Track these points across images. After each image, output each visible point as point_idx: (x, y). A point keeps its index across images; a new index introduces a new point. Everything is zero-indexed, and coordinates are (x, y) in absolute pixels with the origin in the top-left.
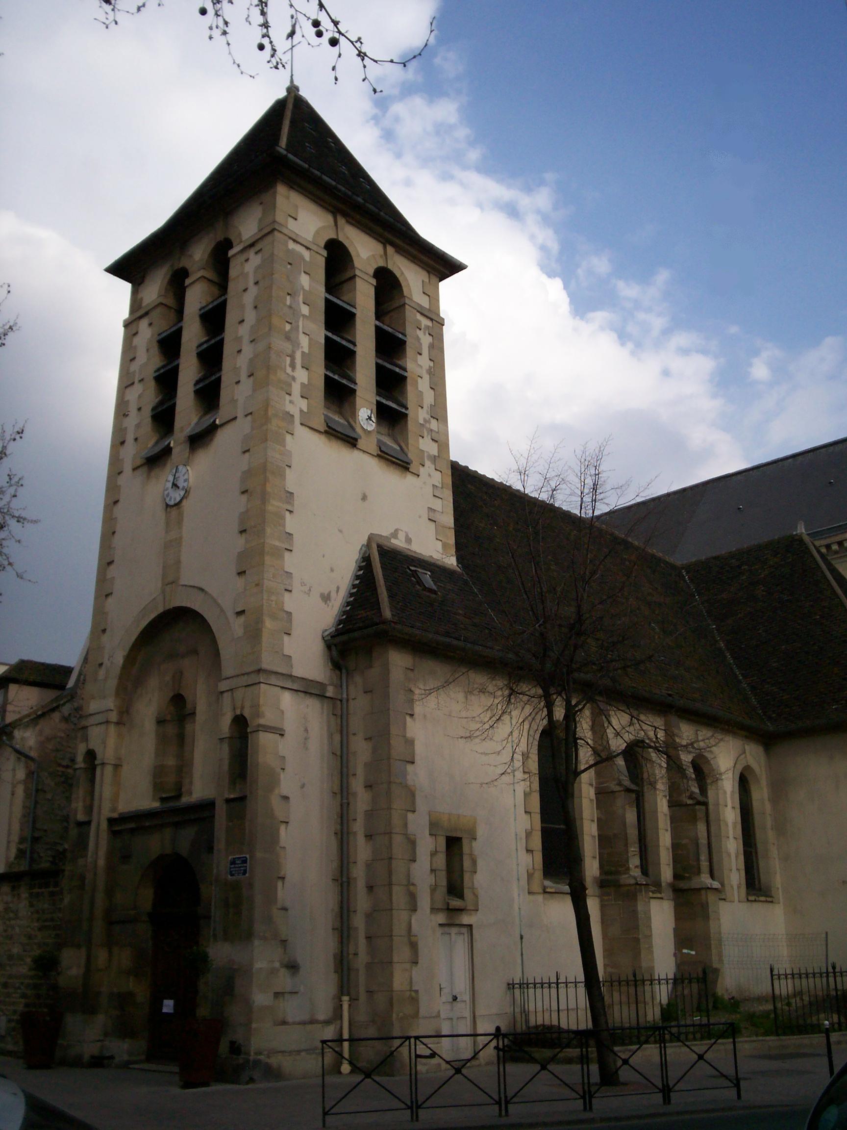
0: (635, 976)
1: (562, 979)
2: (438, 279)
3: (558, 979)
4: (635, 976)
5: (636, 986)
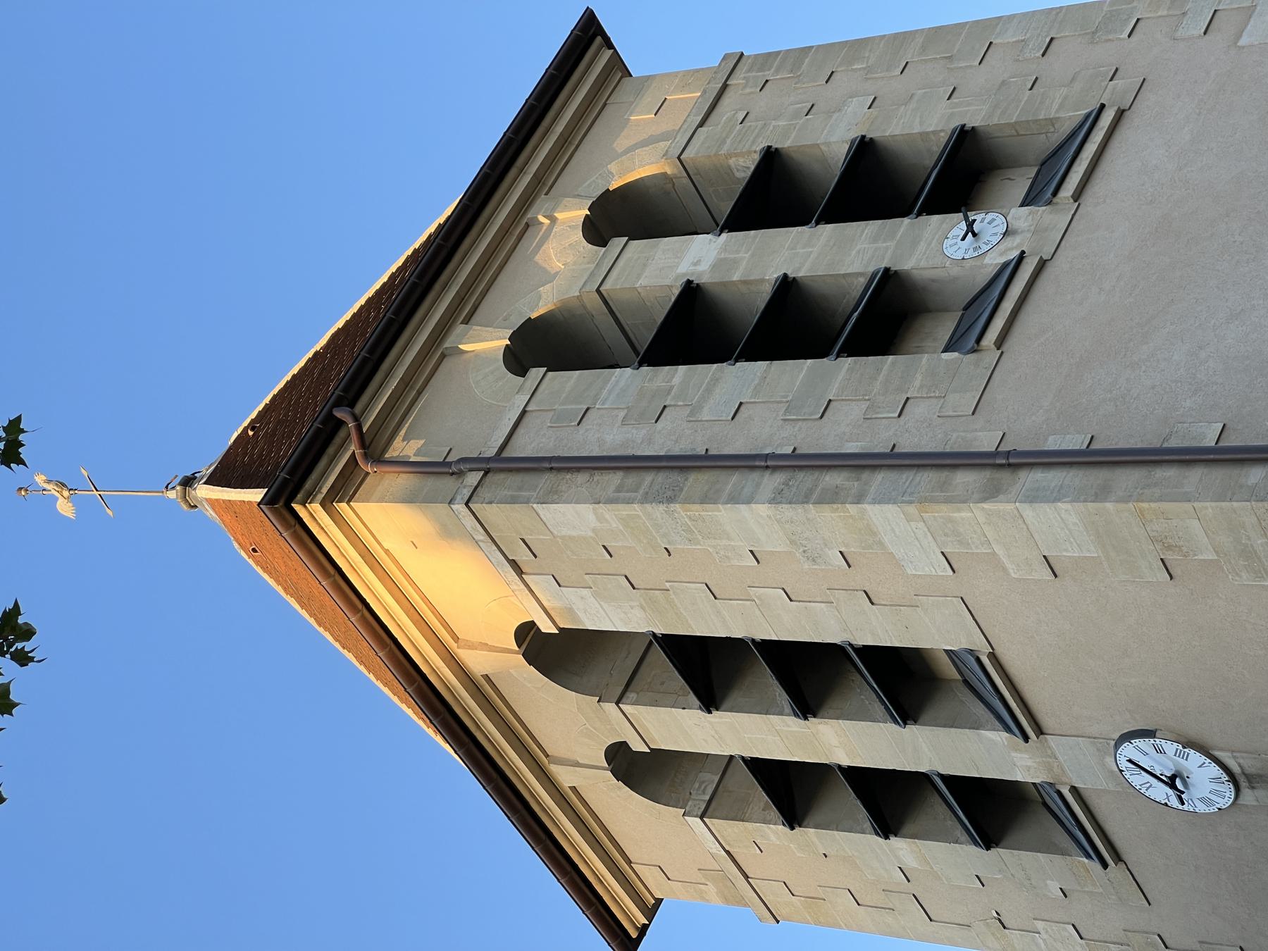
2: (626, 80)
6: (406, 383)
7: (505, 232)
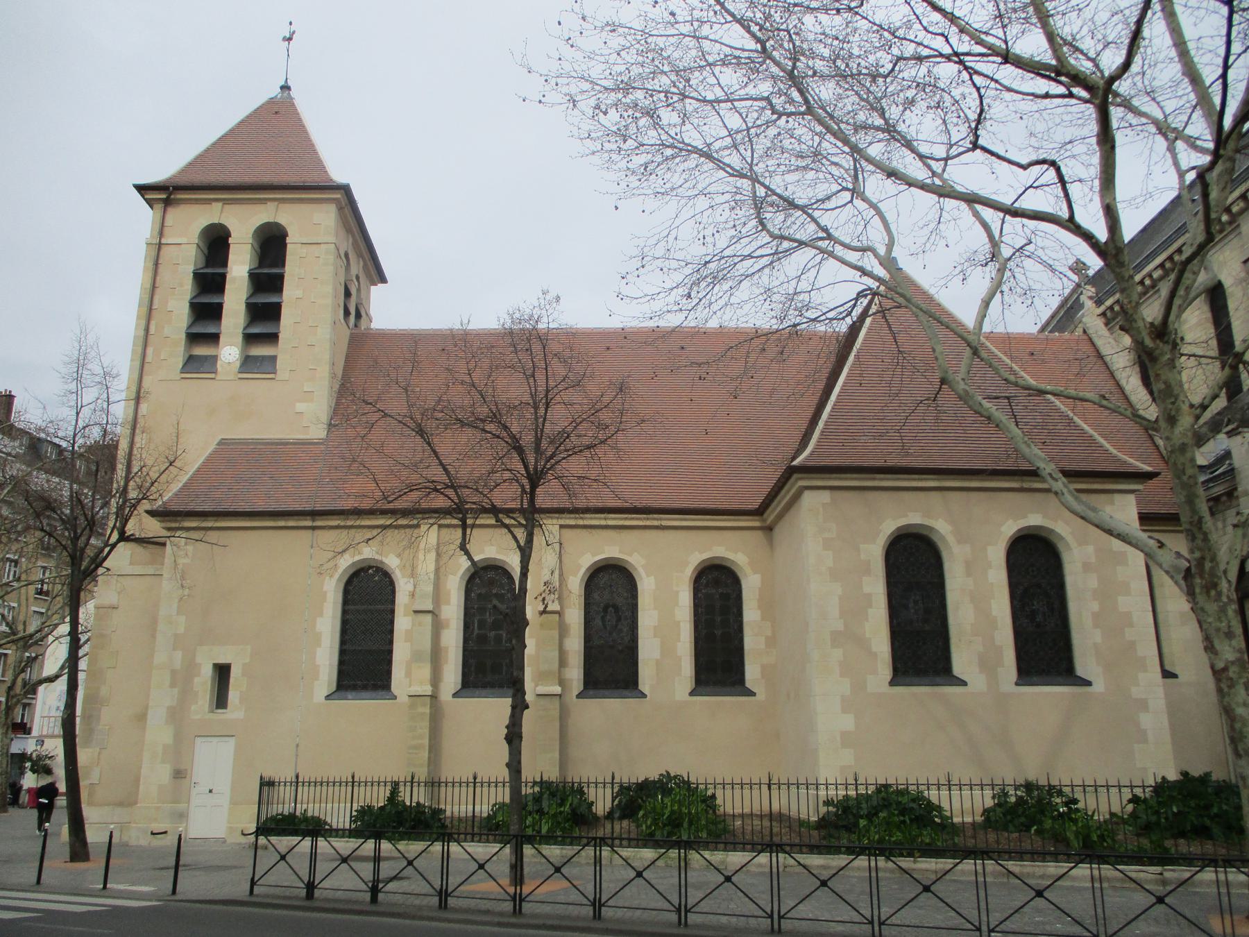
0: (353, 777)
1: (775, 781)
3: (856, 780)
4: (353, 777)
5: (769, 788)
6: (196, 200)
7: (259, 199)
